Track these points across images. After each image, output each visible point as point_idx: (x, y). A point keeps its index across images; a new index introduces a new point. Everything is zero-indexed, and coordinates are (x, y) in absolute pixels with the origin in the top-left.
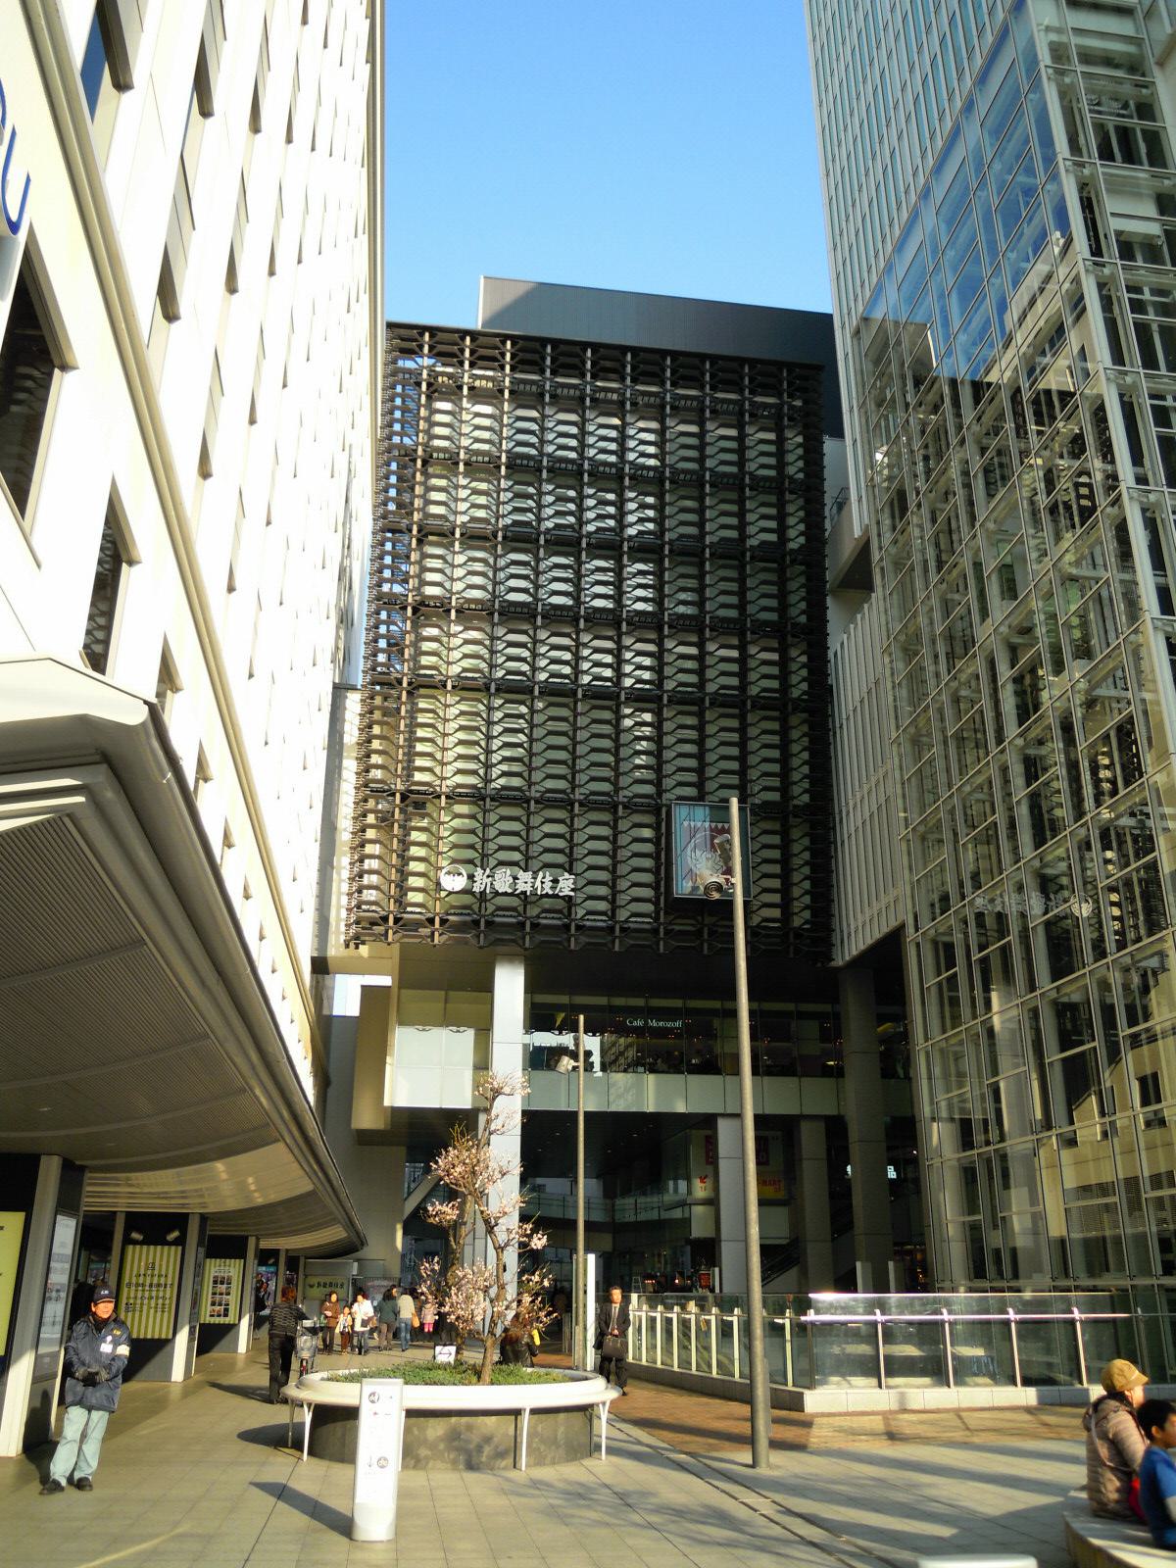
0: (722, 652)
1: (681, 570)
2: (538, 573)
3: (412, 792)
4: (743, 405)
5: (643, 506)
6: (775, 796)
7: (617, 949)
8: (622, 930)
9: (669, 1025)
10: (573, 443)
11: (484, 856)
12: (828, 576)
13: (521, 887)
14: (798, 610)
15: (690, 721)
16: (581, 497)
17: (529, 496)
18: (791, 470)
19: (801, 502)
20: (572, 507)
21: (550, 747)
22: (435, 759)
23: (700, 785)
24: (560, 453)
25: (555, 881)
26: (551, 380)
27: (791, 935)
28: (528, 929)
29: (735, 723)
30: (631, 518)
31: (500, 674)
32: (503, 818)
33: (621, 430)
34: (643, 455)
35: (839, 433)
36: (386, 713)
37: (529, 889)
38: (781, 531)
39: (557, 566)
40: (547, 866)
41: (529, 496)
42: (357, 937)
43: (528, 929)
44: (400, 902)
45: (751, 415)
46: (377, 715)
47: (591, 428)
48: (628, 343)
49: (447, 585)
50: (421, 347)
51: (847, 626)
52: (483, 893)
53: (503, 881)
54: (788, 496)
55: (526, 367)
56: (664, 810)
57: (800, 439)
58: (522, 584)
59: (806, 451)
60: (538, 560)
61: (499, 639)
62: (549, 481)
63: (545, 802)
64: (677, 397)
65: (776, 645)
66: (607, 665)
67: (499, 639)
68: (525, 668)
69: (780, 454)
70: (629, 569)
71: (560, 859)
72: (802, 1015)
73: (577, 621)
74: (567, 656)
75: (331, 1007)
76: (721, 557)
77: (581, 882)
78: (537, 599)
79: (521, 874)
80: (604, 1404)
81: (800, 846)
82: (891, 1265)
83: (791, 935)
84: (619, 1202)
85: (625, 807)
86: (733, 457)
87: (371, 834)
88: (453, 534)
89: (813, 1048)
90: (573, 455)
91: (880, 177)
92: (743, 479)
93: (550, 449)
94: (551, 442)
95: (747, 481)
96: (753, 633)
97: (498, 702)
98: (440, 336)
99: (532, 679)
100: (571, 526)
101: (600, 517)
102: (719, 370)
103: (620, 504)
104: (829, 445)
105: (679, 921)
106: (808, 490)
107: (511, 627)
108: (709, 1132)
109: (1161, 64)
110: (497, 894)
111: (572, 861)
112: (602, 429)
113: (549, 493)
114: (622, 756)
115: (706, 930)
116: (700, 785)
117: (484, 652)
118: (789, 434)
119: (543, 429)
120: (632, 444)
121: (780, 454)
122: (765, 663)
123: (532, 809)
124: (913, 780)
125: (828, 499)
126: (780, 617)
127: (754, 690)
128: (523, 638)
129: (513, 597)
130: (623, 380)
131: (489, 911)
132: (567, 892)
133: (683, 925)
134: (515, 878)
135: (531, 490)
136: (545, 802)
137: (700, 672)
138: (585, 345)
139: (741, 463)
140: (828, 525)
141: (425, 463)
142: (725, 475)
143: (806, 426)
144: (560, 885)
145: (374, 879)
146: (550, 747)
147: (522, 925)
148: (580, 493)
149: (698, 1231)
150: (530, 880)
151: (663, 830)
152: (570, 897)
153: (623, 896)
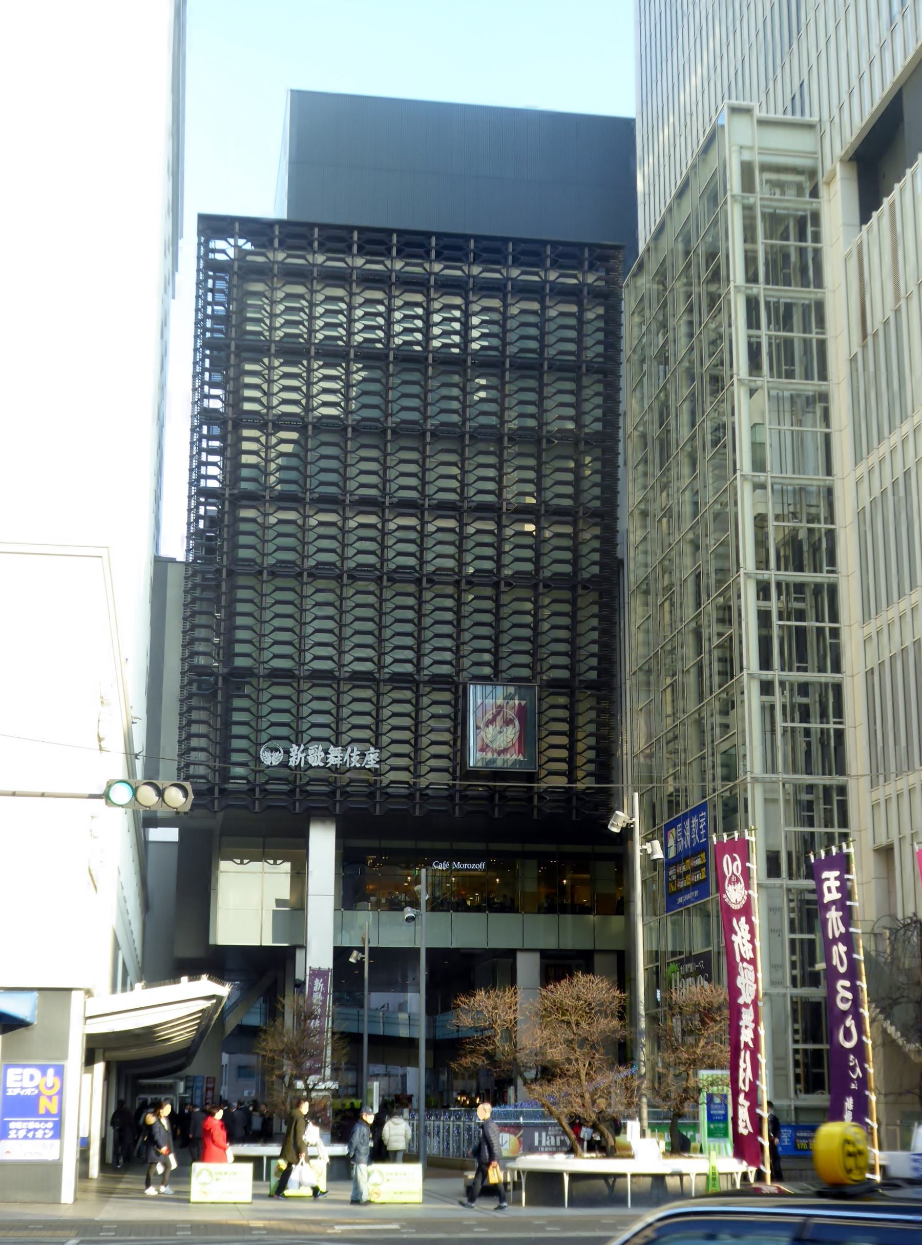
7: (417, 814)
11: (299, 733)
13: (332, 761)
25: (363, 755)
37: (338, 761)
40: (354, 740)
44: (225, 776)
52: (298, 767)
53: (315, 757)
56: (461, 687)
101: (407, 331)
110: (311, 767)
111: (378, 735)
114: (427, 466)
115: (497, 796)
116: (495, 667)
124: (694, 764)
145: (202, 756)
153: (427, 645)
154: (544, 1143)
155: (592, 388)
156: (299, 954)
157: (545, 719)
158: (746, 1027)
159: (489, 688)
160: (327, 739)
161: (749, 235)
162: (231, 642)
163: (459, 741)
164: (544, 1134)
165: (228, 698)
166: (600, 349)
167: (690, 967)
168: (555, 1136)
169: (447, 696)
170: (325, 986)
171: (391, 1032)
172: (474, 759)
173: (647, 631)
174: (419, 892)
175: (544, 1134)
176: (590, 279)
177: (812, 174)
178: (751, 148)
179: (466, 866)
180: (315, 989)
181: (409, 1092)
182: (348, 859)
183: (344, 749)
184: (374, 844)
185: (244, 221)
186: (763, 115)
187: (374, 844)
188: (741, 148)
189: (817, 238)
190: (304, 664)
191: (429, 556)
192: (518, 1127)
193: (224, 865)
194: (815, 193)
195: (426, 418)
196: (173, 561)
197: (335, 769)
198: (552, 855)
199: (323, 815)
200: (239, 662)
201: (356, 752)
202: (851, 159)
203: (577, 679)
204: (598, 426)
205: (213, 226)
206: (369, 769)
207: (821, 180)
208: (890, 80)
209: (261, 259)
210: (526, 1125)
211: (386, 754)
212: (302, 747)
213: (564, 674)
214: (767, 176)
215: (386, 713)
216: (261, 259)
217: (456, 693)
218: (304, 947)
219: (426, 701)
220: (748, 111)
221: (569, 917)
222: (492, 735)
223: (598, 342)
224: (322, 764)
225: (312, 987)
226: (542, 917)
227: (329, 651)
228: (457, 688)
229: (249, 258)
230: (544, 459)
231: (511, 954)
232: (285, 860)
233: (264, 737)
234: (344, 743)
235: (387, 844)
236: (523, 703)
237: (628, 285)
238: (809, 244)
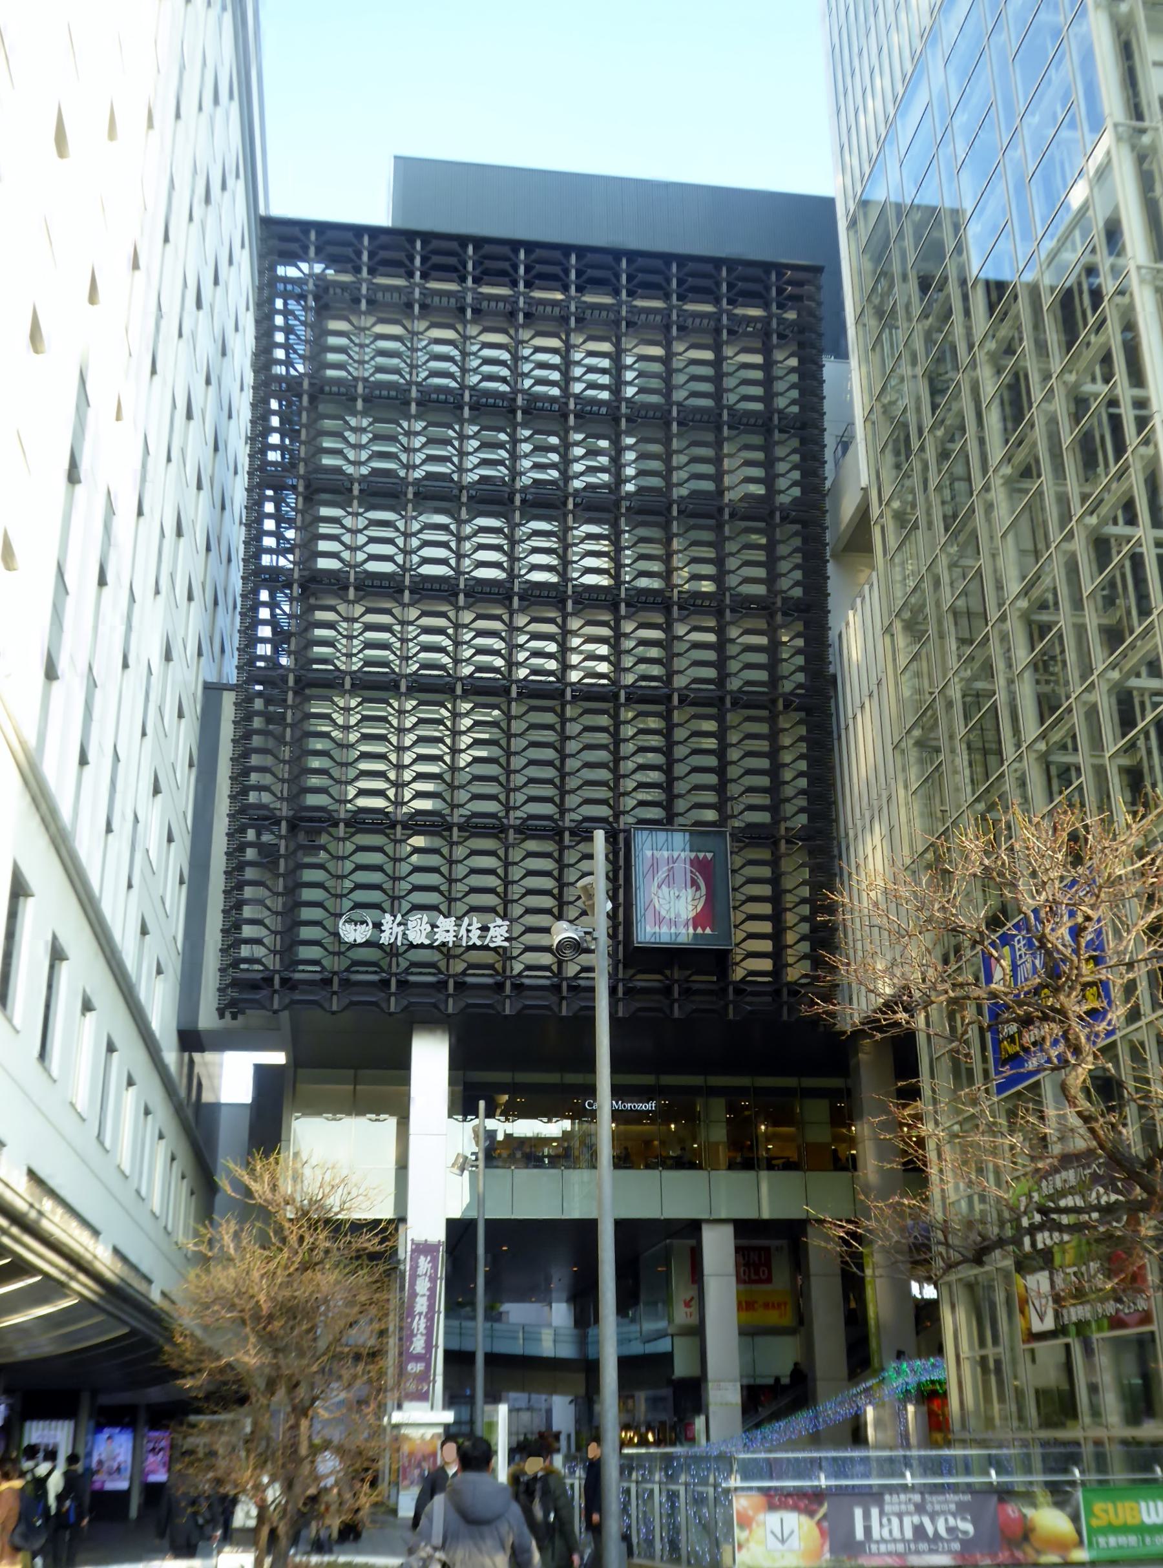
0: (746, 637)
1: (695, 535)
2: (513, 543)
3: (302, 819)
4: (719, 320)
5: (592, 453)
6: (763, 817)
8: (571, 988)
10: (555, 376)
12: (828, 537)
13: (441, 937)
14: (790, 583)
15: (653, 723)
16: (566, 445)
17: (501, 445)
18: (781, 402)
19: (795, 443)
20: (555, 457)
21: (532, 762)
22: (388, 780)
23: (668, 805)
24: (485, 384)
25: (485, 929)
26: (474, 291)
27: (785, 991)
28: (451, 989)
29: (763, 728)
30: (578, 467)
31: (467, 670)
32: (531, 854)
33: (565, 354)
34: (592, 386)
35: (842, 354)
36: (269, 718)
37: (450, 939)
38: (769, 481)
39: (537, 533)
40: (473, 909)
41: (501, 445)
42: (233, 1003)
43: (451, 989)
45: (731, 332)
46: (257, 723)
47: (527, 352)
48: (621, 246)
50: (305, 249)
51: (854, 601)
53: (418, 930)
54: (777, 436)
55: (647, 292)
56: (622, 836)
57: (793, 362)
58: (441, 553)
59: (802, 377)
60: (513, 526)
61: (466, 626)
62: (525, 425)
63: (527, 830)
64: (426, 293)
65: (765, 626)
66: (601, 658)
67: (466, 626)
68: (499, 662)
69: (768, 382)
70: (575, 532)
72: (713, 1092)
73: (563, 602)
74: (552, 647)
75: (215, 1090)
76: (693, 515)
77: (518, 929)
78: (458, 571)
79: (441, 921)
82: (911, 1408)
83: (785, 991)
85: (573, 833)
86: (758, 391)
87: (250, 873)
88: (512, 501)
89: (819, 1134)
90: (555, 391)
91: (891, 18)
92: (720, 415)
93: (578, 388)
94: (475, 370)
95: (725, 417)
96: (733, 611)
97: (410, 705)
98: (590, 256)
99: (508, 677)
100: (553, 482)
101: (591, 470)
102: (739, 279)
103: (564, 449)
104: (830, 367)
105: (639, 977)
106: (804, 428)
107: (370, 605)
108: (693, 1242)
110: (412, 946)
112: (540, 354)
113: (526, 440)
114: (567, 806)
116: (668, 805)
118: (778, 355)
119: (516, 358)
120: (578, 371)
121: (768, 382)
122: (697, 645)
123: (455, 838)
125: (830, 440)
126: (769, 590)
127: (734, 684)
128: (441, 622)
129: (427, 570)
130: (410, 275)
131: (515, 972)
132: (499, 942)
133: (644, 980)
134: (434, 926)
135: (503, 437)
136: (527, 830)
137: (720, 664)
138: (566, 249)
139: (718, 395)
140: (829, 470)
141: (313, 399)
142: (749, 413)
143: (801, 345)
144: (492, 933)
146: (532, 762)
147: (385, 983)
148: (564, 440)
149: (682, 1368)
150: (452, 928)
151: (621, 862)
152: (505, 948)
154: (876, 1534)
159: (662, 836)
163: (621, 891)
164: (875, 1512)
168: (900, 1516)
170: (435, 1268)
171: (532, 1351)
173: (918, 675)
175: (875, 1512)
180: (421, 1271)
181: (555, 1428)
182: (458, 1063)
185: (323, 228)
187: (504, 1077)
190: (404, 804)
191: (572, 801)
192: (818, 1496)
195: (563, 811)
198: (742, 1091)
199: (431, 1021)
201: (476, 925)
203: (783, 826)
206: (495, 949)
210: (841, 1491)
224: (427, 942)
225: (415, 1268)
231: (693, 1228)
232: (392, 1114)
234: (459, 914)
235: (524, 1077)
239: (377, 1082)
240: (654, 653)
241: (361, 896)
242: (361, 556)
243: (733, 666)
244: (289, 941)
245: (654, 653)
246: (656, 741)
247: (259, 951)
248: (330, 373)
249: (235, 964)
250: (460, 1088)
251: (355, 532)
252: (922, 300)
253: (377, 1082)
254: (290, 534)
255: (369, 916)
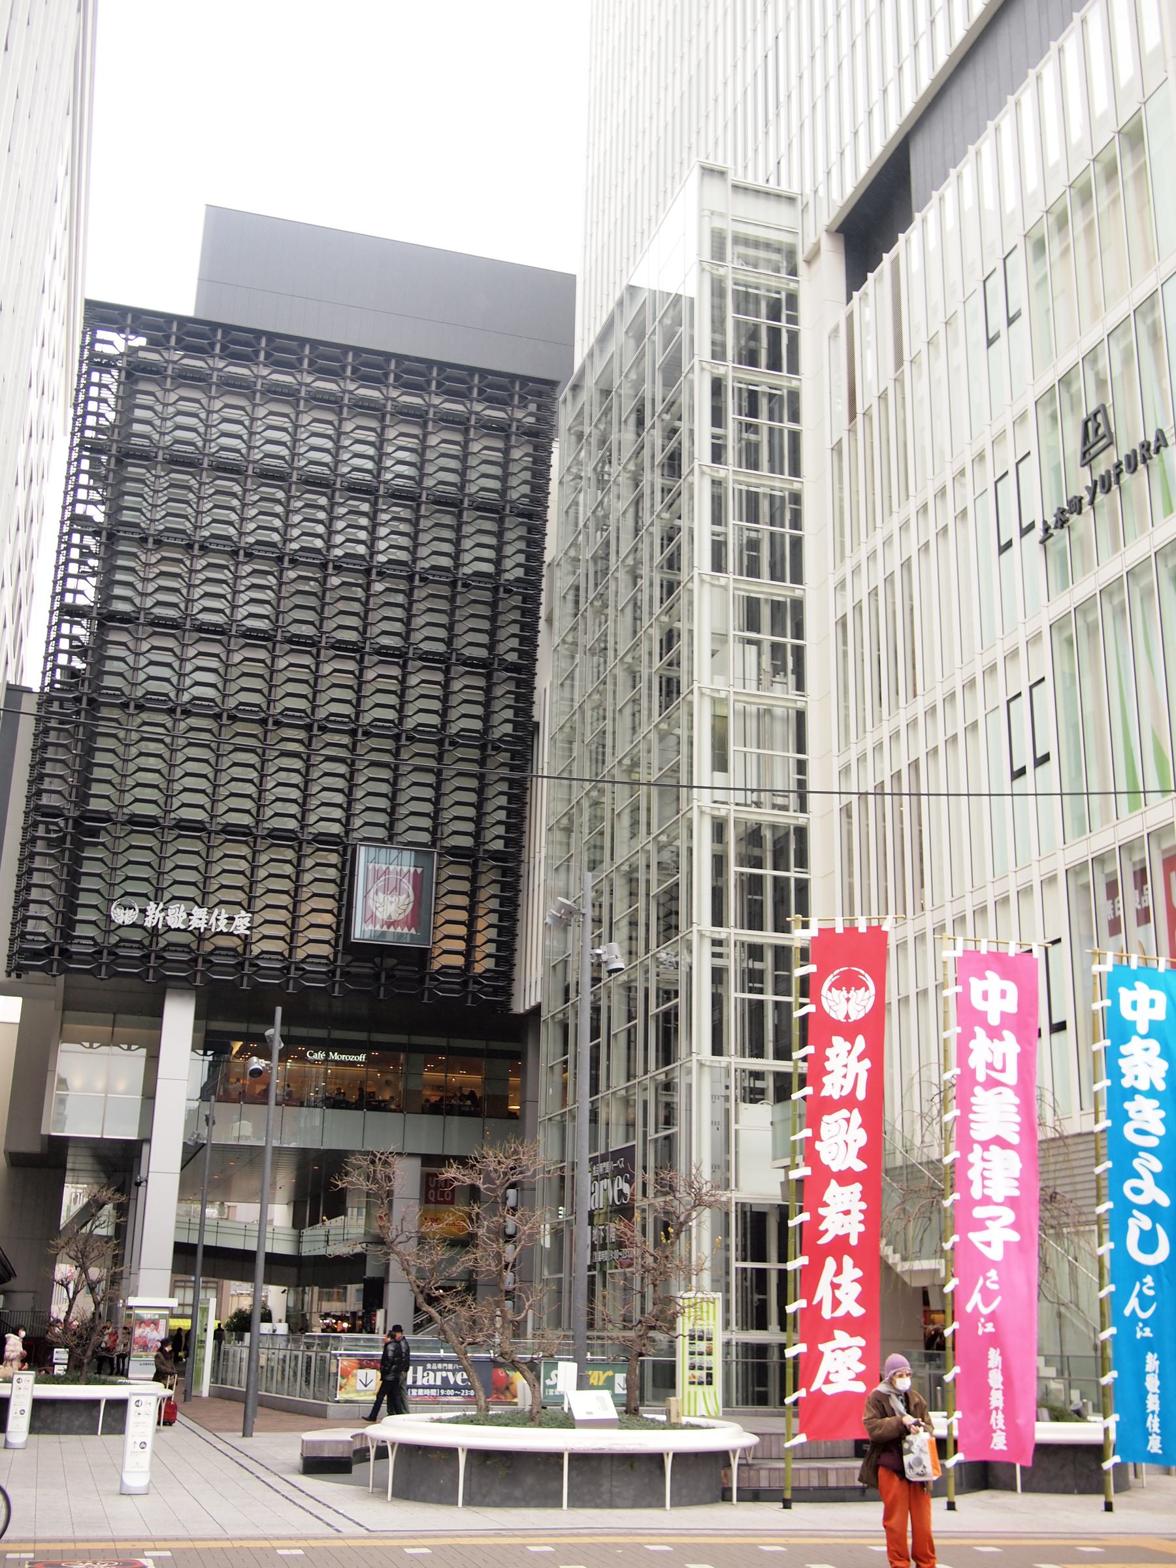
9: (352, 1058)
11: (159, 891)
13: (195, 923)
30: (339, 539)
37: (203, 926)
49: (137, 601)
52: (155, 927)
53: (176, 917)
71: (240, 896)
79: (196, 911)
80: (734, 1451)
81: (489, 892)
84: (307, 1232)
109: (808, 262)
110: (170, 929)
116: (390, 828)
117: (244, 432)
132: (242, 931)
133: (364, 969)
144: (236, 922)
145: (57, 785)
150: (204, 917)
155: (515, 532)
156: (145, 1148)
157: (442, 891)
158: (143, 1445)
160: (192, 899)
161: (718, 418)
162: (87, 782)
165: (79, 845)
166: (526, 489)
167: (607, 1166)
169: (334, 858)
172: (361, 931)
174: (271, 1039)
176: (519, 414)
177: (791, 254)
178: (722, 215)
179: (343, 1057)
183: (210, 911)
184: (242, 1027)
185: (138, 313)
186: (740, 179)
187: (242, 1027)
188: (712, 213)
189: (793, 320)
193: (20, 1000)
194: (793, 272)
196: (29, 691)
197: (200, 936)
199: (184, 985)
200: (95, 805)
201: (224, 915)
202: (838, 231)
204: (520, 572)
205: (101, 315)
206: (238, 936)
207: (800, 258)
208: (893, 128)
209: (154, 357)
211: (258, 919)
212: (161, 906)
213: (467, 842)
214: (742, 250)
215: (262, 873)
216: (154, 357)
217: (343, 855)
218: (149, 1141)
219: (308, 863)
220: (722, 173)
221: (456, 1118)
222: (383, 904)
223: (525, 482)
226: (425, 1117)
227: (201, 799)
228: (345, 849)
229: (142, 354)
230: (465, 519)
233: (118, 892)
236: (419, 870)
237: (565, 401)
238: (783, 324)
239: (139, 1020)
240: (403, 527)
241: (131, 887)
242: (149, 602)
243: (472, 475)
244: (67, 922)
245: (403, 527)
246: (404, 541)
247: (44, 928)
248: (134, 440)
249: (23, 935)
250: (203, 1034)
251: (145, 580)
252: (601, 403)
253: (139, 1020)
254: (93, 562)
255: (136, 903)
